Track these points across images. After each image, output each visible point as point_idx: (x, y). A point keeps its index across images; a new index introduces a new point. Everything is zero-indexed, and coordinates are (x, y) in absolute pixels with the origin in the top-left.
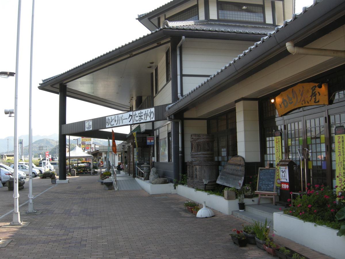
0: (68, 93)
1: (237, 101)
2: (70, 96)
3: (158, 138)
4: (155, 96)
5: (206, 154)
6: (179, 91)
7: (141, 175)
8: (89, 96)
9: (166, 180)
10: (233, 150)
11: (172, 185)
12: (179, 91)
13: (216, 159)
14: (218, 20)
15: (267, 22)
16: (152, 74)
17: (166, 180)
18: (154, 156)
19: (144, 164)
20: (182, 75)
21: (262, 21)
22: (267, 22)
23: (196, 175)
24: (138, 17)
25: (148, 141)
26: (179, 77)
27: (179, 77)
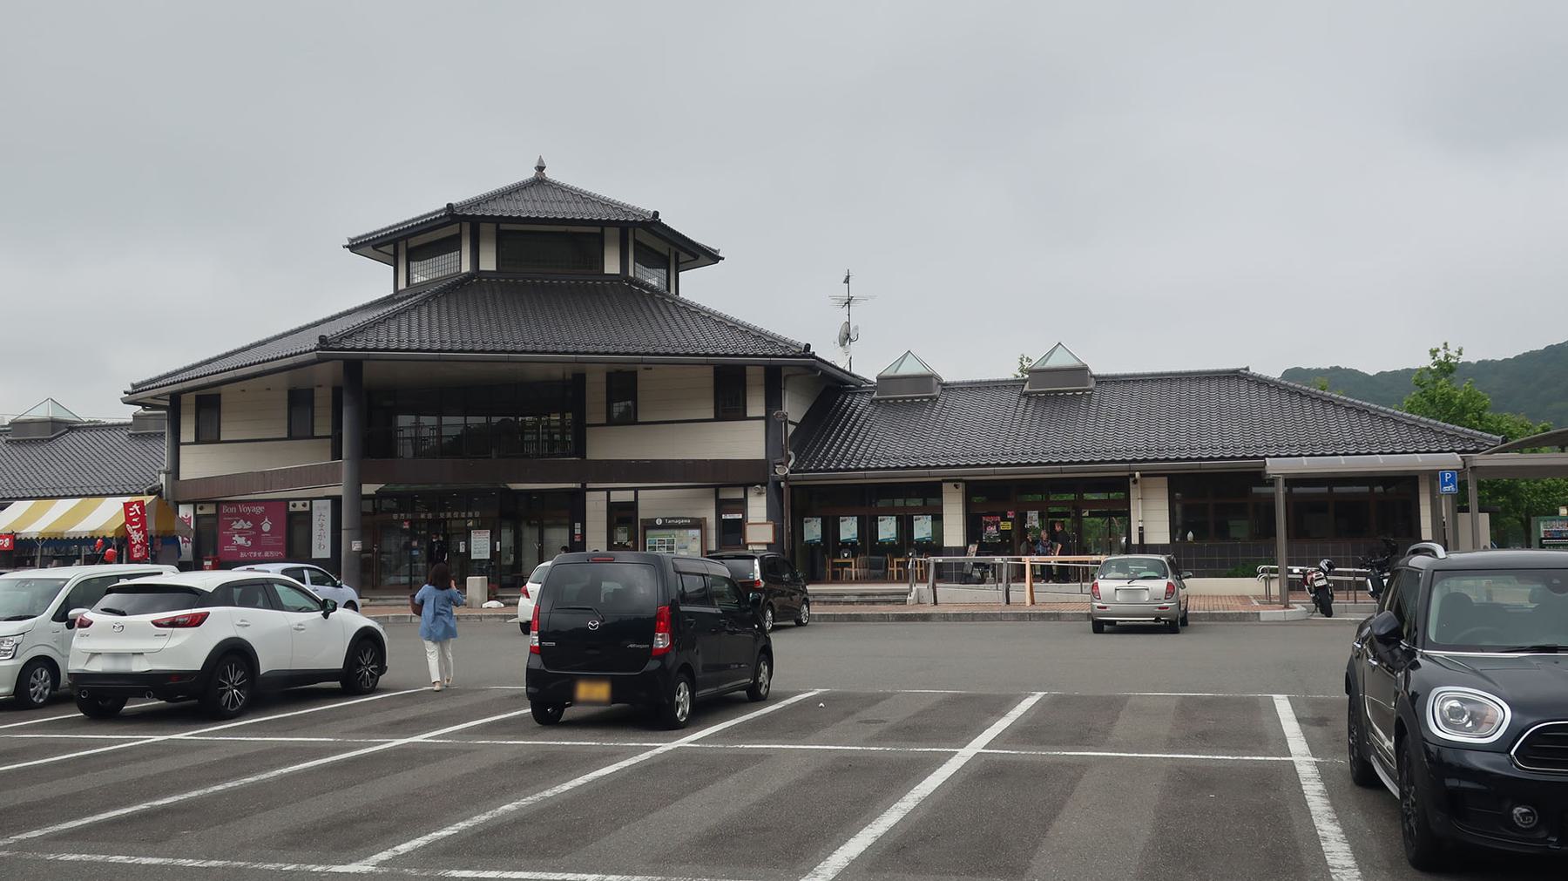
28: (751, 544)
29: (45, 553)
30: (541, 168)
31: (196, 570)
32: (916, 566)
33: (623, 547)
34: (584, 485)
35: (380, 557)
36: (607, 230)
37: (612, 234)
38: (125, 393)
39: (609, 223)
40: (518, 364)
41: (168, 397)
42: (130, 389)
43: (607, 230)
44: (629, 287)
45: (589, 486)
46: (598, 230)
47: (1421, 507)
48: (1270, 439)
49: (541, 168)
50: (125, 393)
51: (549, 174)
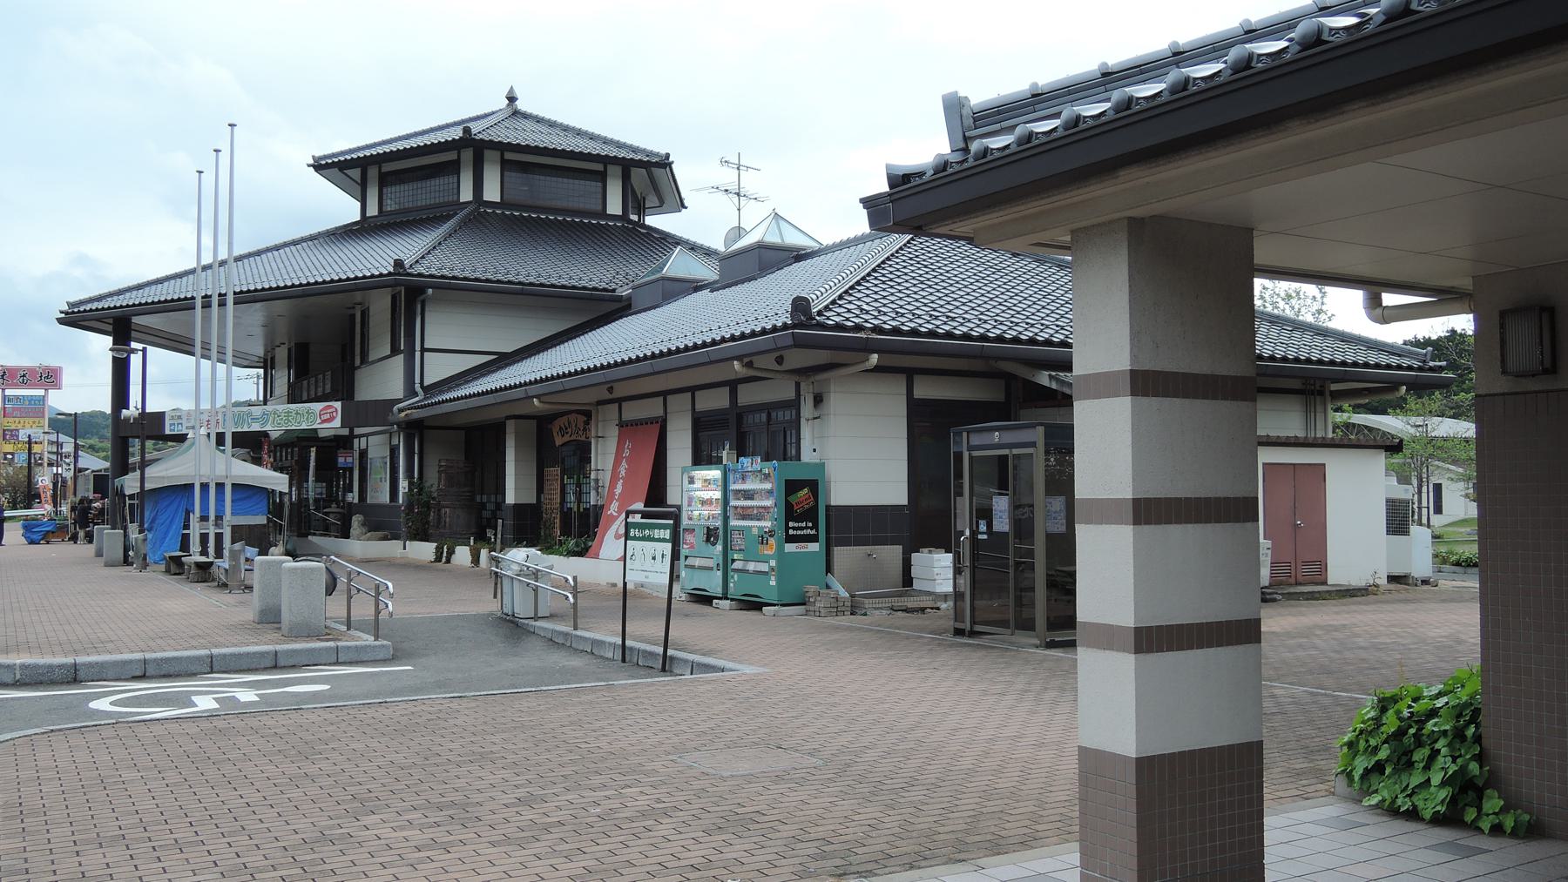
0: (134, 334)
1: (509, 418)
2: (101, 330)
3: (363, 454)
4: (359, 367)
5: (609, 231)
6: (417, 380)
7: (326, 530)
8: (151, 332)
9: (387, 536)
10: (500, 489)
11: (399, 543)
12: (417, 380)
13: (478, 499)
14: (502, 204)
15: (610, 211)
16: (353, 317)
17: (387, 536)
18: (960, 494)
19: (330, 507)
20: (423, 350)
21: (600, 208)
22: (610, 211)
23: (445, 522)
24: (312, 162)
25: (341, 460)
26: (418, 354)
27: (418, 354)
28: (664, 540)
29: (50, 449)
30: (512, 99)
31: (1241, 621)
32: (204, 538)
33: (9, 453)
34: (352, 431)
35: (435, 508)
36: (611, 168)
37: (614, 172)
38: (62, 312)
39: (615, 160)
40: (340, 296)
41: (111, 321)
42: (66, 308)
43: (611, 168)
44: (634, 228)
45: (358, 431)
46: (599, 167)
47: (1478, 641)
48: (591, 353)
49: (512, 99)
50: (62, 312)
51: (521, 105)
